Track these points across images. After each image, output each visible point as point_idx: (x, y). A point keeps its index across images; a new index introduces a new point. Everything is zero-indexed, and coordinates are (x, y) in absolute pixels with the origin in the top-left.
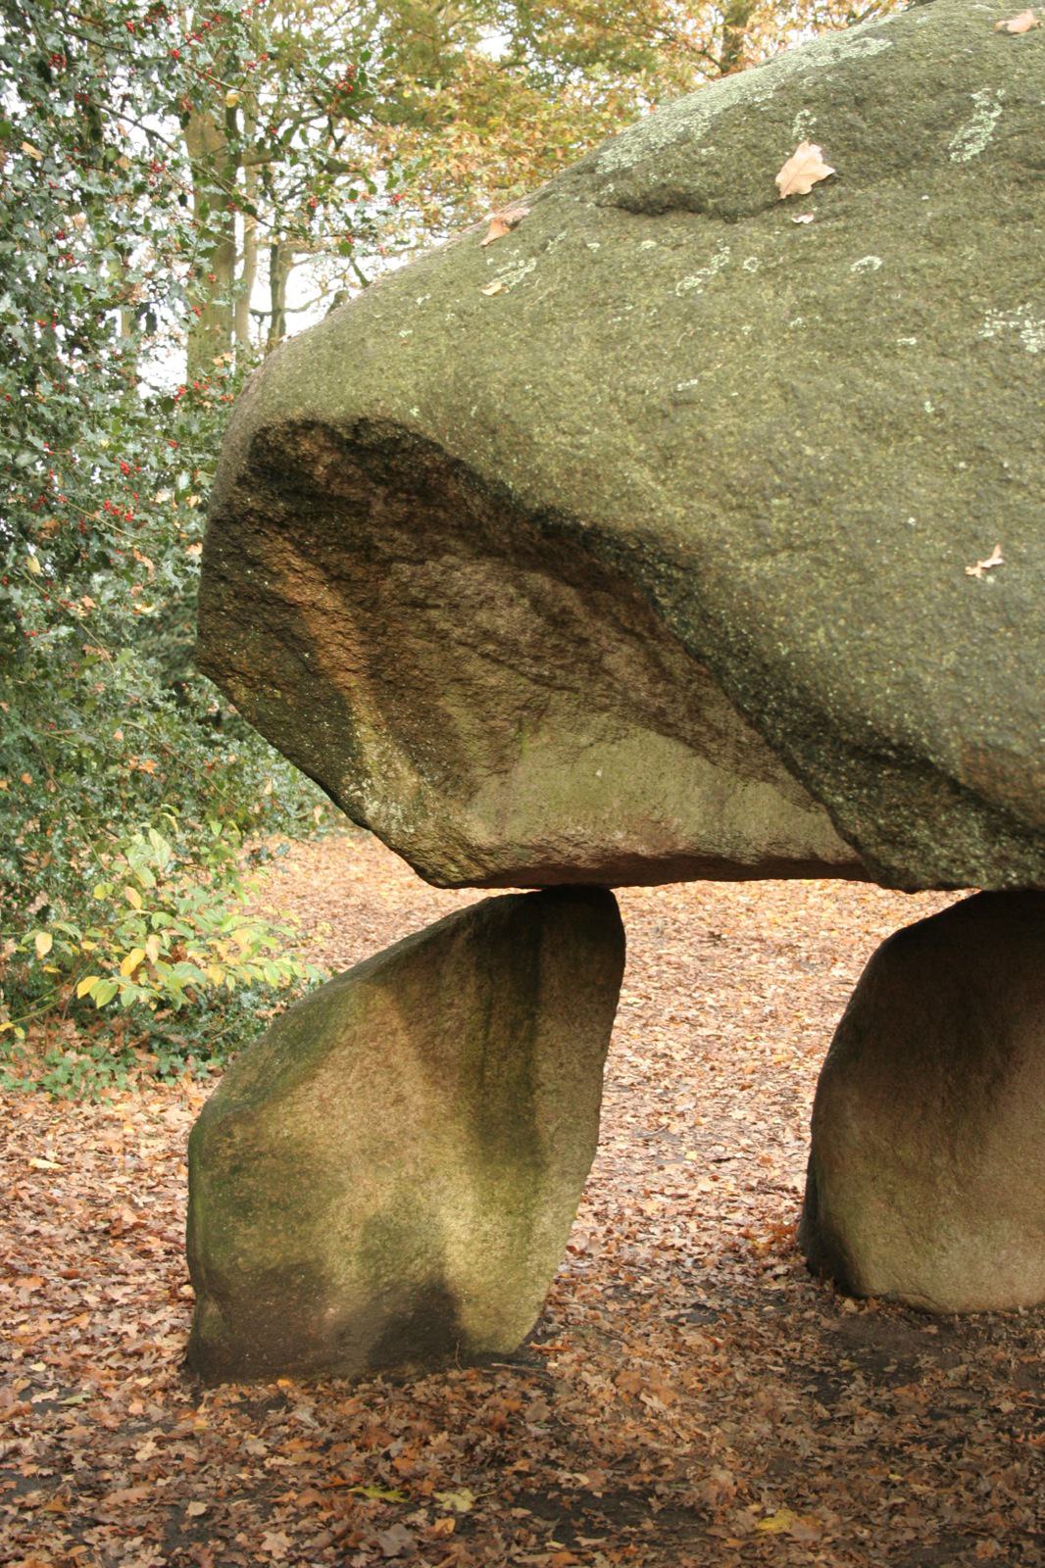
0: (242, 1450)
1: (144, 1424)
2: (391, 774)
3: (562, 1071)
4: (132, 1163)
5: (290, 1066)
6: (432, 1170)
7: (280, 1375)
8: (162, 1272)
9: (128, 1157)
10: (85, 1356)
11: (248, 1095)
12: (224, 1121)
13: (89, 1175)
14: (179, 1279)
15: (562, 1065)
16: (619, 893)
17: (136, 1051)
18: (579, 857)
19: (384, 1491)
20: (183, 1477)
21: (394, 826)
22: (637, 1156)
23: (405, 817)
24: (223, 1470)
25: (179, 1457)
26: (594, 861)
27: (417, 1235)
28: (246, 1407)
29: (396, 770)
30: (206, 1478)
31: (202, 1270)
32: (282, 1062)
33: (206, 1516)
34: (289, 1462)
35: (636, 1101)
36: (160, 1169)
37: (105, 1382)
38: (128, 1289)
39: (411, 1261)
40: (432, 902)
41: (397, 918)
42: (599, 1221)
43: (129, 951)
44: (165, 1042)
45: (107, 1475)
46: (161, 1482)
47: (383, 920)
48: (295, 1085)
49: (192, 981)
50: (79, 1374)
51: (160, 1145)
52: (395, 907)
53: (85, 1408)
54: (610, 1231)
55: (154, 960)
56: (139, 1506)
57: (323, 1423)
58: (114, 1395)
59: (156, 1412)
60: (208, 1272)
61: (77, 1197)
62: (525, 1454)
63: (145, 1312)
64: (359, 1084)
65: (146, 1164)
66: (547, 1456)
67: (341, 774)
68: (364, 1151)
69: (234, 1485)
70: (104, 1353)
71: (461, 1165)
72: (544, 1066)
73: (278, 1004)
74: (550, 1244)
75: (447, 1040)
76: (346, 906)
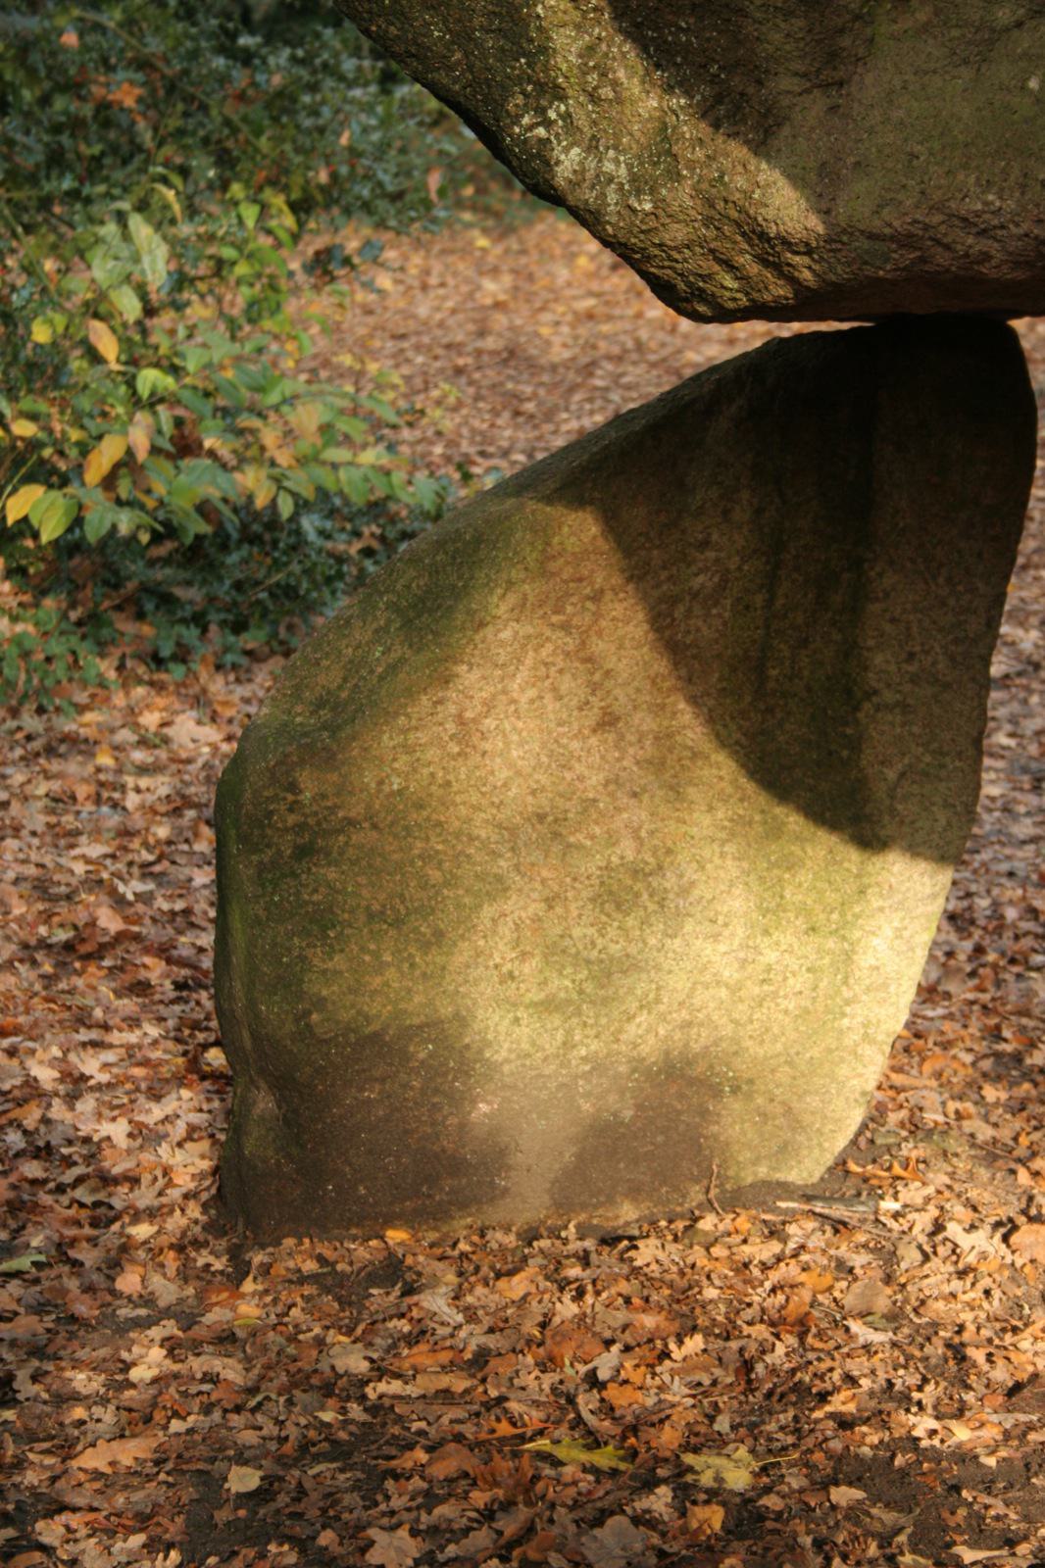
0: (324, 1366)
1: (143, 1312)
2: (606, 92)
3: (913, 668)
4: (114, 820)
5: (402, 661)
6: (669, 852)
7: (389, 1221)
8: (171, 1023)
9: (105, 809)
10: (35, 1182)
11: (325, 714)
12: (279, 763)
13: (36, 842)
14: (201, 1037)
15: (911, 656)
16: (1019, 325)
17: (114, 616)
18: (986, 257)
19: (589, 1448)
20: (217, 1415)
21: (612, 197)
22: (1022, 809)
23: (634, 179)
24: (290, 1402)
25: (211, 1378)
26: (1017, 264)
27: (641, 970)
28: (328, 1280)
29: (615, 84)
30: (260, 1418)
31: (246, 1034)
32: (387, 651)
33: (261, 1496)
34: (411, 1390)
35: (1015, 707)
36: (162, 832)
37: (71, 1232)
38: (110, 1056)
39: (630, 1018)
40: (630, 344)
41: (571, 376)
42: (959, 930)
43: (100, 437)
44: (166, 601)
45: (79, 1413)
46: (176, 1426)
47: (546, 378)
48: (411, 694)
49: (214, 494)
50: (23, 1215)
51: (161, 786)
52: (567, 354)
53: (36, 1281)
54: (979, 950)
55: (142, 455)
56: (137, 1475)
57: (471, 1314)
58: (87, 1256)
59: (166, 1290)
60: (255, 1036)
61: (16, 882)
62: (851, 1380)
63: (142, 1099)
64: (532, 693)
65: (138, 821)
66: (890, 1384)
67: (505, 89)
68: (541, 818)
69: (312, 1434)
70: (69, 1176)
71: (723, 843)
72: (878, 659)
73: (366, 531)
74: (885, 986)
75: (698, 610)
76: (479, 353)
